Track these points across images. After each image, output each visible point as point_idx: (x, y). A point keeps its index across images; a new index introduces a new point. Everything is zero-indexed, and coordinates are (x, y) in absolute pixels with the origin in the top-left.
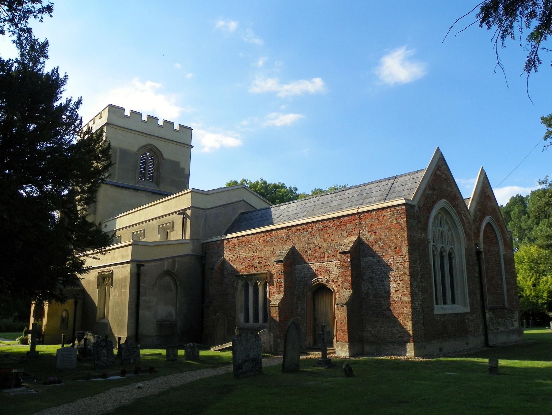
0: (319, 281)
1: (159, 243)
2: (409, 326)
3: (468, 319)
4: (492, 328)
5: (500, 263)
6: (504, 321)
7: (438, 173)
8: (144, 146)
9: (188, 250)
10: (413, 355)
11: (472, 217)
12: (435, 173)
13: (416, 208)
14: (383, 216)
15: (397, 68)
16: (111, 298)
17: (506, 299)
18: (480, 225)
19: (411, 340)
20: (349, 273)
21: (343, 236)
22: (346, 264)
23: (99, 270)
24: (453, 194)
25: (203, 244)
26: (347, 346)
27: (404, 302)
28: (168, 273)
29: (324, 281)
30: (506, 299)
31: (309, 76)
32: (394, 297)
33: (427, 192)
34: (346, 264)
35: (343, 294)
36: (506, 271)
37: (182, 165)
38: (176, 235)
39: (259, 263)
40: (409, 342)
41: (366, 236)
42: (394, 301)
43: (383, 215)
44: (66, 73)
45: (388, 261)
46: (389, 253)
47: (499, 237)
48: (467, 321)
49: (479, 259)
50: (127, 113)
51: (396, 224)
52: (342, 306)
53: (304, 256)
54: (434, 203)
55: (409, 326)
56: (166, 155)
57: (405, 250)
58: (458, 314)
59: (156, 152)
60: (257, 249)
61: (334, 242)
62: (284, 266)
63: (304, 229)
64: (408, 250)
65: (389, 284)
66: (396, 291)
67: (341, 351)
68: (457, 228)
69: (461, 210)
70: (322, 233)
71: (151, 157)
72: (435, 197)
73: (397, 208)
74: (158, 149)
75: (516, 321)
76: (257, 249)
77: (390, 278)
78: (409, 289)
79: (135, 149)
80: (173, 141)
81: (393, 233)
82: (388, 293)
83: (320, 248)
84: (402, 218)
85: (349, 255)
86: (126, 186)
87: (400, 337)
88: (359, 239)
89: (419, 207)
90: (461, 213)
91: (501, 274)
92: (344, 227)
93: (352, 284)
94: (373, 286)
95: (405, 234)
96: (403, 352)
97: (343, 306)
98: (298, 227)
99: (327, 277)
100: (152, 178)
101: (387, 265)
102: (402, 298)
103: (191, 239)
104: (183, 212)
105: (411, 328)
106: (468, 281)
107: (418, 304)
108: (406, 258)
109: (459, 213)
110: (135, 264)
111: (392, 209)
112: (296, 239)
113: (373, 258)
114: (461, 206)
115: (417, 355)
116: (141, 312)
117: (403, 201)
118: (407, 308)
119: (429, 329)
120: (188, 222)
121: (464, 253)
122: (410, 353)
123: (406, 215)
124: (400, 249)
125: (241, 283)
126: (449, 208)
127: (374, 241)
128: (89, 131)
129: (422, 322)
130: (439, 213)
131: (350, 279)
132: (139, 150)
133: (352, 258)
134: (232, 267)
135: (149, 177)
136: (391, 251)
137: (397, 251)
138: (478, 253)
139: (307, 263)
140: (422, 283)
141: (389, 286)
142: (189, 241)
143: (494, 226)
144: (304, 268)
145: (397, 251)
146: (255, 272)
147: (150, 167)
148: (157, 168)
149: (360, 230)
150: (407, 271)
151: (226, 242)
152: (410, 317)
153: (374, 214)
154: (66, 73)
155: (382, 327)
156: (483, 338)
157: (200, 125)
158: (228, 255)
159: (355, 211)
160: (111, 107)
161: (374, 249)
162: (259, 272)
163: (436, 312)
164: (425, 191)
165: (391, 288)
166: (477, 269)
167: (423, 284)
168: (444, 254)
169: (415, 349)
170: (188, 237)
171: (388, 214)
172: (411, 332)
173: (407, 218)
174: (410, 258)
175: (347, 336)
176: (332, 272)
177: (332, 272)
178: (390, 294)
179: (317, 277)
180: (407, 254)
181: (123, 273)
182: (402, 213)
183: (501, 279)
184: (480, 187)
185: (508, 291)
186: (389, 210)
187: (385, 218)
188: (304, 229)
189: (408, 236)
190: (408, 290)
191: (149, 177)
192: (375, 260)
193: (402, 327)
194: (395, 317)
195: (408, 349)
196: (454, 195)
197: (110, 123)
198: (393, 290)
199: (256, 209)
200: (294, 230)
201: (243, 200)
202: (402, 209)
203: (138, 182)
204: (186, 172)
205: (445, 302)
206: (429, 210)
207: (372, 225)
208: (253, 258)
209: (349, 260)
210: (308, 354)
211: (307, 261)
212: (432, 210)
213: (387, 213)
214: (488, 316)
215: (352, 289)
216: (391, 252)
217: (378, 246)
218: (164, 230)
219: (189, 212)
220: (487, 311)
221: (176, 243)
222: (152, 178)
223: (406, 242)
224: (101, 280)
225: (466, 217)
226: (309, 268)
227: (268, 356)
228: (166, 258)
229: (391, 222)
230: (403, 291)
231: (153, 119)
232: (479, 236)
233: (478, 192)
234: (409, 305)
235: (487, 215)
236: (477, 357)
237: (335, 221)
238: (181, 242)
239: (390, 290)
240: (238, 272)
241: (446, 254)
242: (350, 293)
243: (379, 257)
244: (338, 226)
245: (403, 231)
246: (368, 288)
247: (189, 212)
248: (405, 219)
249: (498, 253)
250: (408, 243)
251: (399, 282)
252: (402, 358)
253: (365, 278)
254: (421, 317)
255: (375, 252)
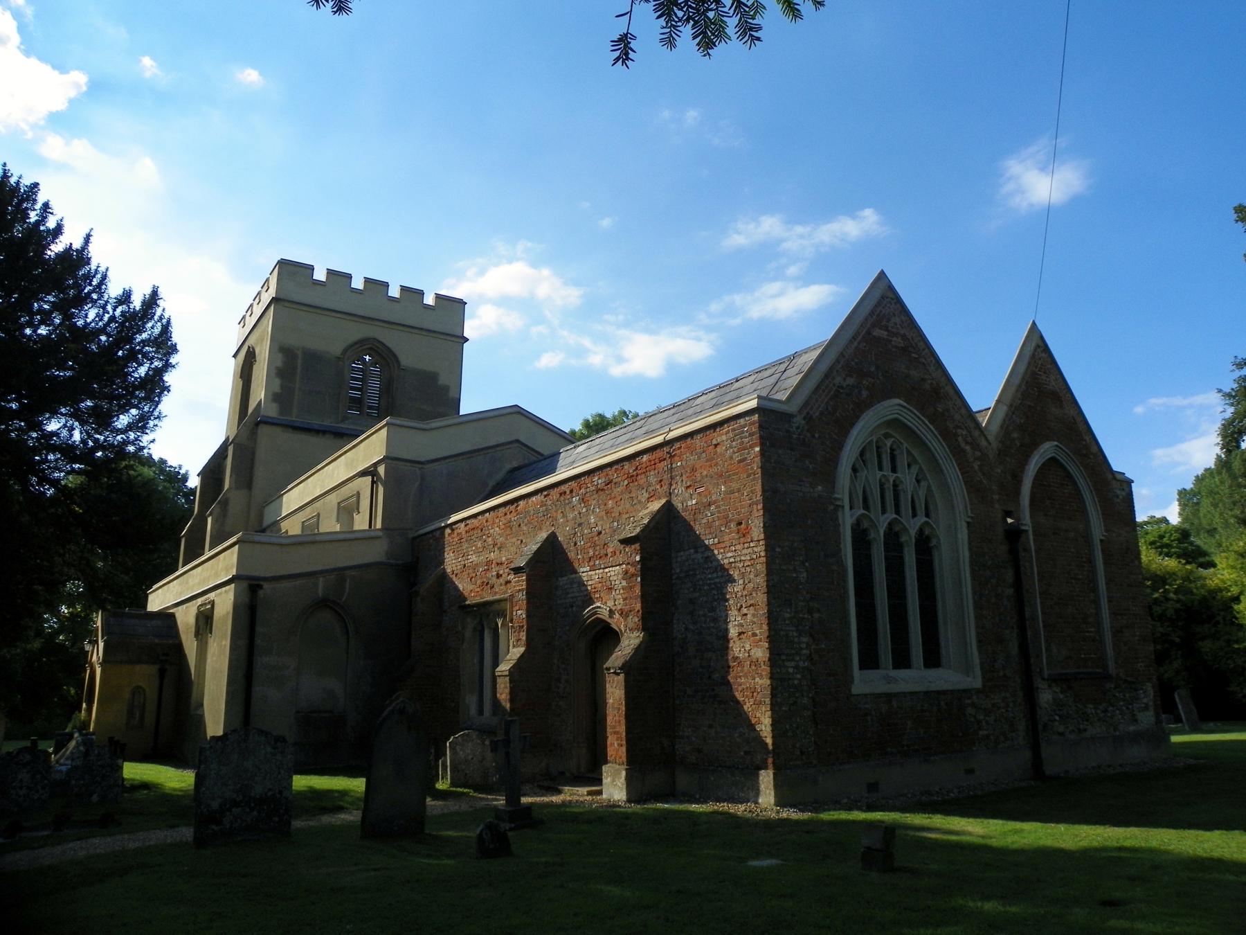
0: (595, 613)
1: (300, 539)
2: (764, 725)
3: (973, 705)
4: (1061, 729)
5: (1091, 561)
6: (1106, 711)
7: (877, 332)
8: (356, 343)
9: (376, 553)
10: (772, 801)
11: (995, 445)
12: (869, 333)
13: (799, 420)
14: (716, 446)
15: (1041, 184)
16: (209, 661)
17: (1110, 652)
18: (1023, 465)
19: (770, 760)
20: (638, 590)
21: (640, 502)
22: (632, 570)
23: (200, 601)
24: (927, 386)
25: (414, 538)
26: (624, 773)
27: (755, 663)
28: (323, 604)
29: (604, 614)
30: (1110, 652)
31: (850, 209)
32: (737, 649)
33: (838, 380)
34: (632, 570)
35: (630, 641)
36: (1109, 581)
37: (443, 380)
38: (361, 522)
39: (499, 576)
40: (766, 768)
41: (686, 501)
42: (735, 659)
43: (714, 442)
44: (5, 165)
45: (725, 557)
46: (726, 538)
47: (1087, 496)
48: (970, 711)
49: (1014, 553)
50: (320, 275)
51: (740, 461)
52: (615, 673)
53: (571, 555)
54: (861, 407)
55: (764, 725)
56: (405, 360)
57: (757, 529)
58: (938, 692)
59: (384, 356)
60: (495, 545)
61: (625, 516)
62: (528, 580)
63: (571, 491)
64: (764, 526)
65: (727, 616)
66: (740, 634)
67: (614, 787)
68: (942, 470)
69: (957, 427)
70: (603, 496)
71: (374, 364)
72: (865, 393)
73: (742, 421)
74: (388, 348)
75: (1146, 708)
76: (495, 545)
77: (727, 600)
78: (765, 627)
79: (336, 349)
80: (421, 329)
81: (734, 485)
82: (725, 638)
83: (600, 533)
84: (752, 447)
85: (637, 546)
86: (316, 427)
87: (746, 753)
88: (668, 508)
89: (808, 418)
90: (956, 435)
91: (1094, 589)
92: (642, 480)
93: (644, 619)
94: (695, 623)
95: (759, 487)
96: (752, 794)
97: (618, 674)
98: (563, 488)
99: (610, 603)
100: (378, 409)
101: (722, 566)
102: (752, 653)
103: (384, 528)
104: (370, 472)
105: (769, 729)
106: (977, 606)
107: (796, 667)
108: (760, 549)
109: (948, 435)
110: (245, 584)
111: (733, 425)
112: (560, 516)
113: (696, 552)
114: (957, 417)
115: (781, 802)
116: (258, 690)
117: (753, 404)
118: (761, 677)
119: (829, 734)
120: (381, 489)
121: (963, 534)
122: (767, 797)
123: (761, 437)
124: (748, 524)
125: (471, 623)
126: (913, 419)
127: (697, 511)
128: (126, 298)
129: (807, 713)
130: (887, 436)
131: (638, 606)
132: (345, 351)
133: (643, 552)
134: (456, 588)
135: (370, 408)
136: (731, 532)
137: (744, 534)
138: (1014, 535)
139: (576, 572)
140: (810, 611)
141: (727, 623)
142: (380, 534)
143: (1072, 469)
144: (572, 583)
145: (744, 534)
146: (490, 598)
147: (374, 385)
148: (388, 388)
149: (671, 485)
150: (761, 581)
151: (448, 531)
152: (768, 701)
153: (698, 441)
154: (5, 165)
155: (710, 726)
156: (1028, 754)
157: (621, 317)
158: (451, 562)
159: (659, 440)
160: (283, 264)
161: (698, 529)
162: (497, 597)
163: (857, 688)
164: (827, 376)
165: (730, 626)
166: (1009, 575)
167: (816, 615)
168: (904, 539)
169: (777, 786)
170: (379, 526)
171: (724, 437)
172: (769, 741)
173: (762, 445)
174: (769, 548)
175: (624, 749)
176: (611, 588)
177: (611, 588)
178: (728, 641)
179: (593, 603)
180: (762, 536)
181: (225, 602)
182: (751, 435)
183: (1096, 602)
184: (1022, 369)
185: (1117, 633)
186: (726, 428)
187: (718, 450)
188: (571, 491)
189: (764, 491)
190: (762, 630)
191: (370, 408)
192: (699, 556)
193: (752, 727)
194: (738, 702)
195: (762, 787)
196: (933, 389)
197: (282, 297)
198: (733, 632)
199: (542, 455)
200: (555, 493)
201: (518, 441)
202: (751, 424)
203: (345, 419)
204: (452, 394)
205: (901, 661)
206: (845, 426)
207: (694, 470)
208: (489, 563)
209: (638, 558)
210: (559, 792)
211: (576, 565)
212: (853, 425)
213: (721, 436)
214: (1046, 697)
215: (643, 630)
216: (730, 535)
217: (704, 521)
218: (347, 510)
219: (381, 470)
220: (1041, 685)
221: (365, 538)
222: (378, 409)
223: (760, 506)
224: (202, 623)
225: (975, 445)
226: (581, 584)
227: (463, 794)
228: (321, 572)
229: (731, 458)
230: (754, 635)
231: (376, 286)
232: (1018, 492)
233: (1017, 381)
234: (765, 670)
235: (1048, 439)
236: (948, 812)
237: (627, 465)
238: (367, 535)
239: (727, 630)
240: (465, 599)
241: (909, 539)
242: (637, 642)
243: (707, 548)
244: (632, 478)
245: (754, 479)
246: (686, 629)
247: (381, 470)
248: (757, 449)
249: (1087, 538)
250: (764, 508)
251: (745, 611)
252: (740, 809)
253: (679, 602)
254: (805, 700)
255: (698, 537)
